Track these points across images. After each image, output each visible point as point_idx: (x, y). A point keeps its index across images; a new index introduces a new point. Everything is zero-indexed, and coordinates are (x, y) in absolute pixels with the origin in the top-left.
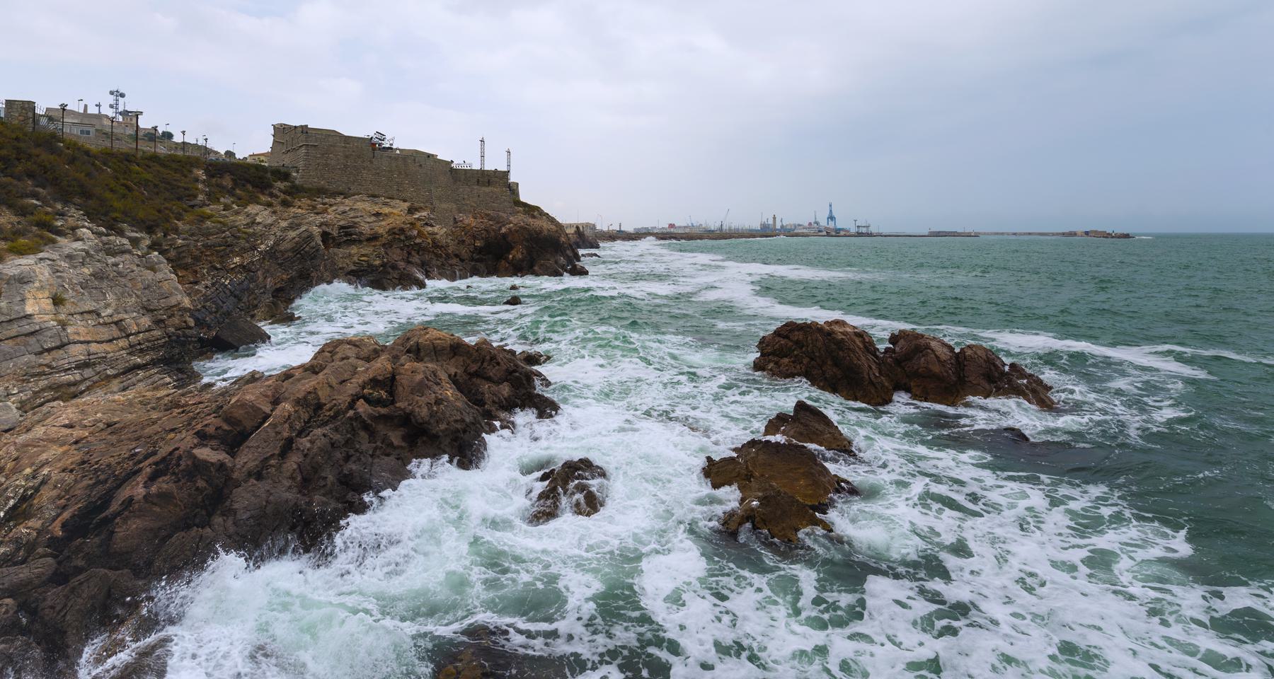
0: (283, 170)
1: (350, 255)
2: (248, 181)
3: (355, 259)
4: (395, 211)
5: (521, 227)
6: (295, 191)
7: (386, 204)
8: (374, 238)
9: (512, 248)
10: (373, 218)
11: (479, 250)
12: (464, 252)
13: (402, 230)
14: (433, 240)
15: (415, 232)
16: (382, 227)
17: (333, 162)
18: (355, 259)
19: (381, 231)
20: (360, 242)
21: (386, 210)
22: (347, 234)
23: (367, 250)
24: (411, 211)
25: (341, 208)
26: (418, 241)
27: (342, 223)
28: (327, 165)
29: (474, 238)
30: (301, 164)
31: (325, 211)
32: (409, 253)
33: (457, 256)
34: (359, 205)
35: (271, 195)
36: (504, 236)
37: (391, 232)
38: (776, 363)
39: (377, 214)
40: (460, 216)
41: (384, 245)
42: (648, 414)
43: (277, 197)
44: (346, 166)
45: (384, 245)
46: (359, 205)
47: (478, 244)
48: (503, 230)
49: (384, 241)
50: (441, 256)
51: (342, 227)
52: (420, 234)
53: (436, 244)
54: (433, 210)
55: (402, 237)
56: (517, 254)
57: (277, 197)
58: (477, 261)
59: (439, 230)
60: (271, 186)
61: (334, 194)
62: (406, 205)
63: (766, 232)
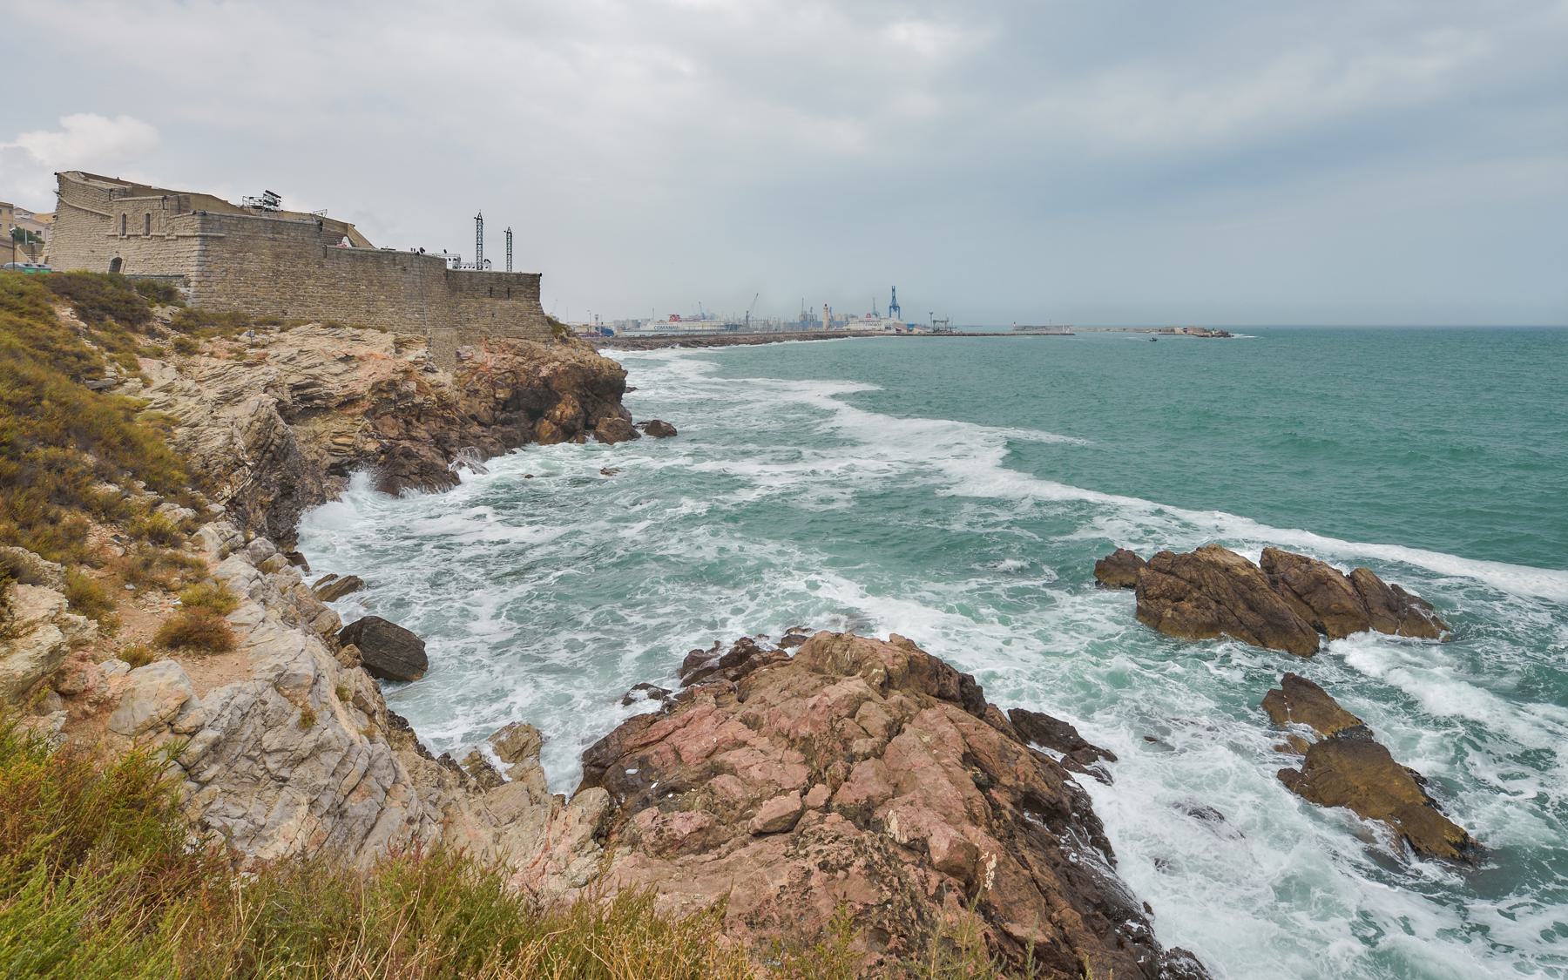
0: (161, 284)
1: (316, 436)
2: (105, 309)
3: (327, 441)
4: (376, 351)
5: (572, 366)
6: (192, 322)
7: (355, 338)
8: (350, 401)
9: (559, 400)
10: (341, 367)
11: (505, 405)
12: (481, 407)
13: (393, 384)
14: (440, 399)
15: (413, 386)
16: (361, 380)
17: (253, 267)
18: (327, 441)
19: (361, 389)
20: (327, 409)
21: (360, 350)
22: (305, 398)
23: (339, 424)
24: (400, 345)
25: (285, 352)
26: (419, 399)
27: (294, 379)
28: (242, 272)
29: (494, 385)
30: (192, 271)
31: (261, 360)
32: (408, 423)
33: (474, 417)
34: (312, 344)
35: (151, 333)
36: (546, 381)
37: (377, 388)
38: (1175, 609)
39: (347, 359)
40: (466, 350)
41: (365, 414)
42: (1510, 949)
43: (164, 336)
44: (277, 273)
45: (365, 414)
46: (312, 344)
47: (501, 394)
48: (545, 372)
49: (367, 405)
50: (453, 422)
51: (295, 387)
52: (421, 388)
53: (444, 404)
54: (429, 343)
55: (393, 396)
56: (566, 410)
57: (164, 336)
58: (504, 423)
59: (444, 377)
60: (148, 317)
61: (264, 324)
62: (389, 338)
63: (808, 330)
